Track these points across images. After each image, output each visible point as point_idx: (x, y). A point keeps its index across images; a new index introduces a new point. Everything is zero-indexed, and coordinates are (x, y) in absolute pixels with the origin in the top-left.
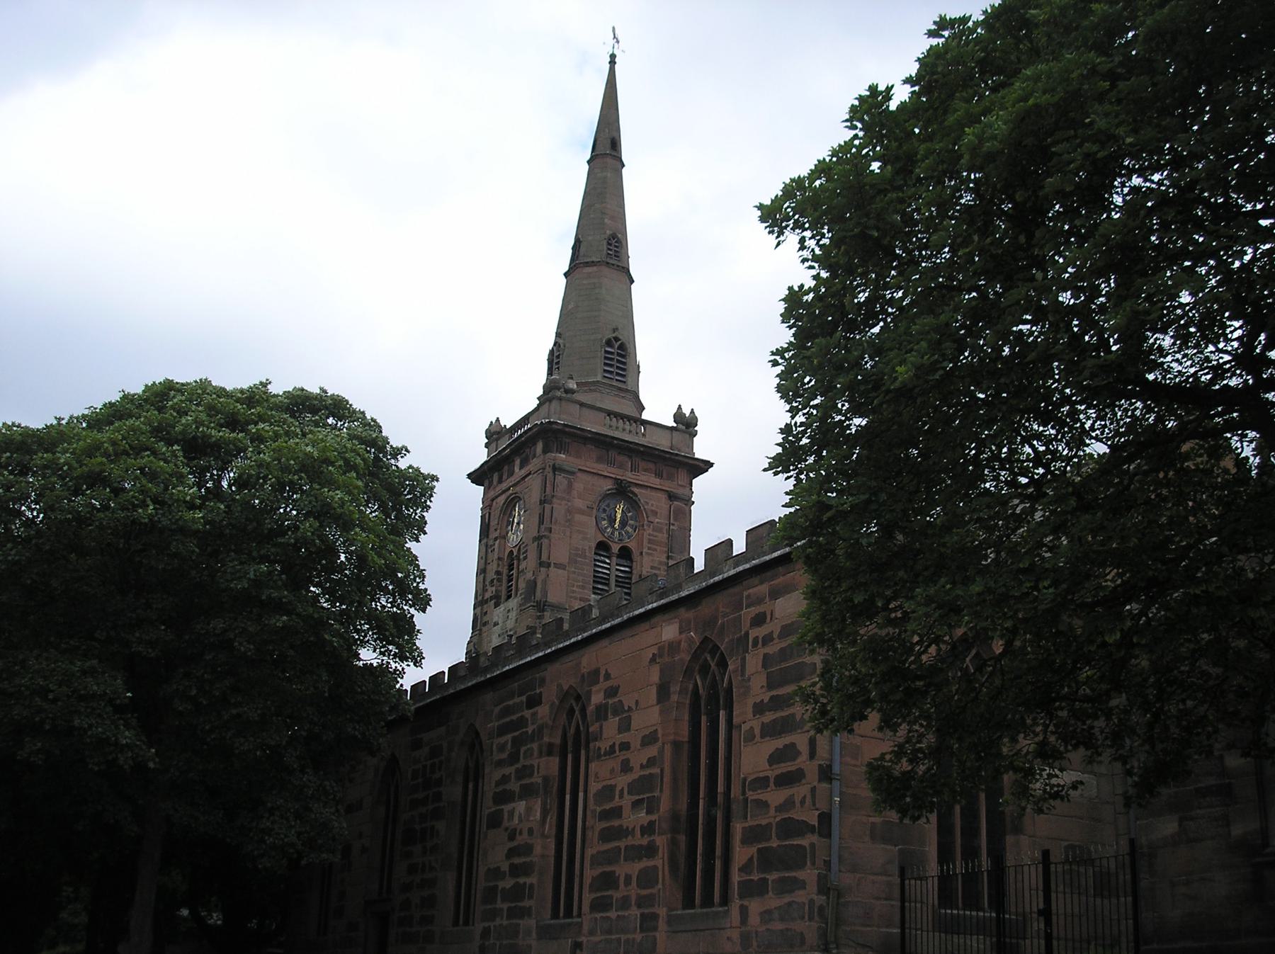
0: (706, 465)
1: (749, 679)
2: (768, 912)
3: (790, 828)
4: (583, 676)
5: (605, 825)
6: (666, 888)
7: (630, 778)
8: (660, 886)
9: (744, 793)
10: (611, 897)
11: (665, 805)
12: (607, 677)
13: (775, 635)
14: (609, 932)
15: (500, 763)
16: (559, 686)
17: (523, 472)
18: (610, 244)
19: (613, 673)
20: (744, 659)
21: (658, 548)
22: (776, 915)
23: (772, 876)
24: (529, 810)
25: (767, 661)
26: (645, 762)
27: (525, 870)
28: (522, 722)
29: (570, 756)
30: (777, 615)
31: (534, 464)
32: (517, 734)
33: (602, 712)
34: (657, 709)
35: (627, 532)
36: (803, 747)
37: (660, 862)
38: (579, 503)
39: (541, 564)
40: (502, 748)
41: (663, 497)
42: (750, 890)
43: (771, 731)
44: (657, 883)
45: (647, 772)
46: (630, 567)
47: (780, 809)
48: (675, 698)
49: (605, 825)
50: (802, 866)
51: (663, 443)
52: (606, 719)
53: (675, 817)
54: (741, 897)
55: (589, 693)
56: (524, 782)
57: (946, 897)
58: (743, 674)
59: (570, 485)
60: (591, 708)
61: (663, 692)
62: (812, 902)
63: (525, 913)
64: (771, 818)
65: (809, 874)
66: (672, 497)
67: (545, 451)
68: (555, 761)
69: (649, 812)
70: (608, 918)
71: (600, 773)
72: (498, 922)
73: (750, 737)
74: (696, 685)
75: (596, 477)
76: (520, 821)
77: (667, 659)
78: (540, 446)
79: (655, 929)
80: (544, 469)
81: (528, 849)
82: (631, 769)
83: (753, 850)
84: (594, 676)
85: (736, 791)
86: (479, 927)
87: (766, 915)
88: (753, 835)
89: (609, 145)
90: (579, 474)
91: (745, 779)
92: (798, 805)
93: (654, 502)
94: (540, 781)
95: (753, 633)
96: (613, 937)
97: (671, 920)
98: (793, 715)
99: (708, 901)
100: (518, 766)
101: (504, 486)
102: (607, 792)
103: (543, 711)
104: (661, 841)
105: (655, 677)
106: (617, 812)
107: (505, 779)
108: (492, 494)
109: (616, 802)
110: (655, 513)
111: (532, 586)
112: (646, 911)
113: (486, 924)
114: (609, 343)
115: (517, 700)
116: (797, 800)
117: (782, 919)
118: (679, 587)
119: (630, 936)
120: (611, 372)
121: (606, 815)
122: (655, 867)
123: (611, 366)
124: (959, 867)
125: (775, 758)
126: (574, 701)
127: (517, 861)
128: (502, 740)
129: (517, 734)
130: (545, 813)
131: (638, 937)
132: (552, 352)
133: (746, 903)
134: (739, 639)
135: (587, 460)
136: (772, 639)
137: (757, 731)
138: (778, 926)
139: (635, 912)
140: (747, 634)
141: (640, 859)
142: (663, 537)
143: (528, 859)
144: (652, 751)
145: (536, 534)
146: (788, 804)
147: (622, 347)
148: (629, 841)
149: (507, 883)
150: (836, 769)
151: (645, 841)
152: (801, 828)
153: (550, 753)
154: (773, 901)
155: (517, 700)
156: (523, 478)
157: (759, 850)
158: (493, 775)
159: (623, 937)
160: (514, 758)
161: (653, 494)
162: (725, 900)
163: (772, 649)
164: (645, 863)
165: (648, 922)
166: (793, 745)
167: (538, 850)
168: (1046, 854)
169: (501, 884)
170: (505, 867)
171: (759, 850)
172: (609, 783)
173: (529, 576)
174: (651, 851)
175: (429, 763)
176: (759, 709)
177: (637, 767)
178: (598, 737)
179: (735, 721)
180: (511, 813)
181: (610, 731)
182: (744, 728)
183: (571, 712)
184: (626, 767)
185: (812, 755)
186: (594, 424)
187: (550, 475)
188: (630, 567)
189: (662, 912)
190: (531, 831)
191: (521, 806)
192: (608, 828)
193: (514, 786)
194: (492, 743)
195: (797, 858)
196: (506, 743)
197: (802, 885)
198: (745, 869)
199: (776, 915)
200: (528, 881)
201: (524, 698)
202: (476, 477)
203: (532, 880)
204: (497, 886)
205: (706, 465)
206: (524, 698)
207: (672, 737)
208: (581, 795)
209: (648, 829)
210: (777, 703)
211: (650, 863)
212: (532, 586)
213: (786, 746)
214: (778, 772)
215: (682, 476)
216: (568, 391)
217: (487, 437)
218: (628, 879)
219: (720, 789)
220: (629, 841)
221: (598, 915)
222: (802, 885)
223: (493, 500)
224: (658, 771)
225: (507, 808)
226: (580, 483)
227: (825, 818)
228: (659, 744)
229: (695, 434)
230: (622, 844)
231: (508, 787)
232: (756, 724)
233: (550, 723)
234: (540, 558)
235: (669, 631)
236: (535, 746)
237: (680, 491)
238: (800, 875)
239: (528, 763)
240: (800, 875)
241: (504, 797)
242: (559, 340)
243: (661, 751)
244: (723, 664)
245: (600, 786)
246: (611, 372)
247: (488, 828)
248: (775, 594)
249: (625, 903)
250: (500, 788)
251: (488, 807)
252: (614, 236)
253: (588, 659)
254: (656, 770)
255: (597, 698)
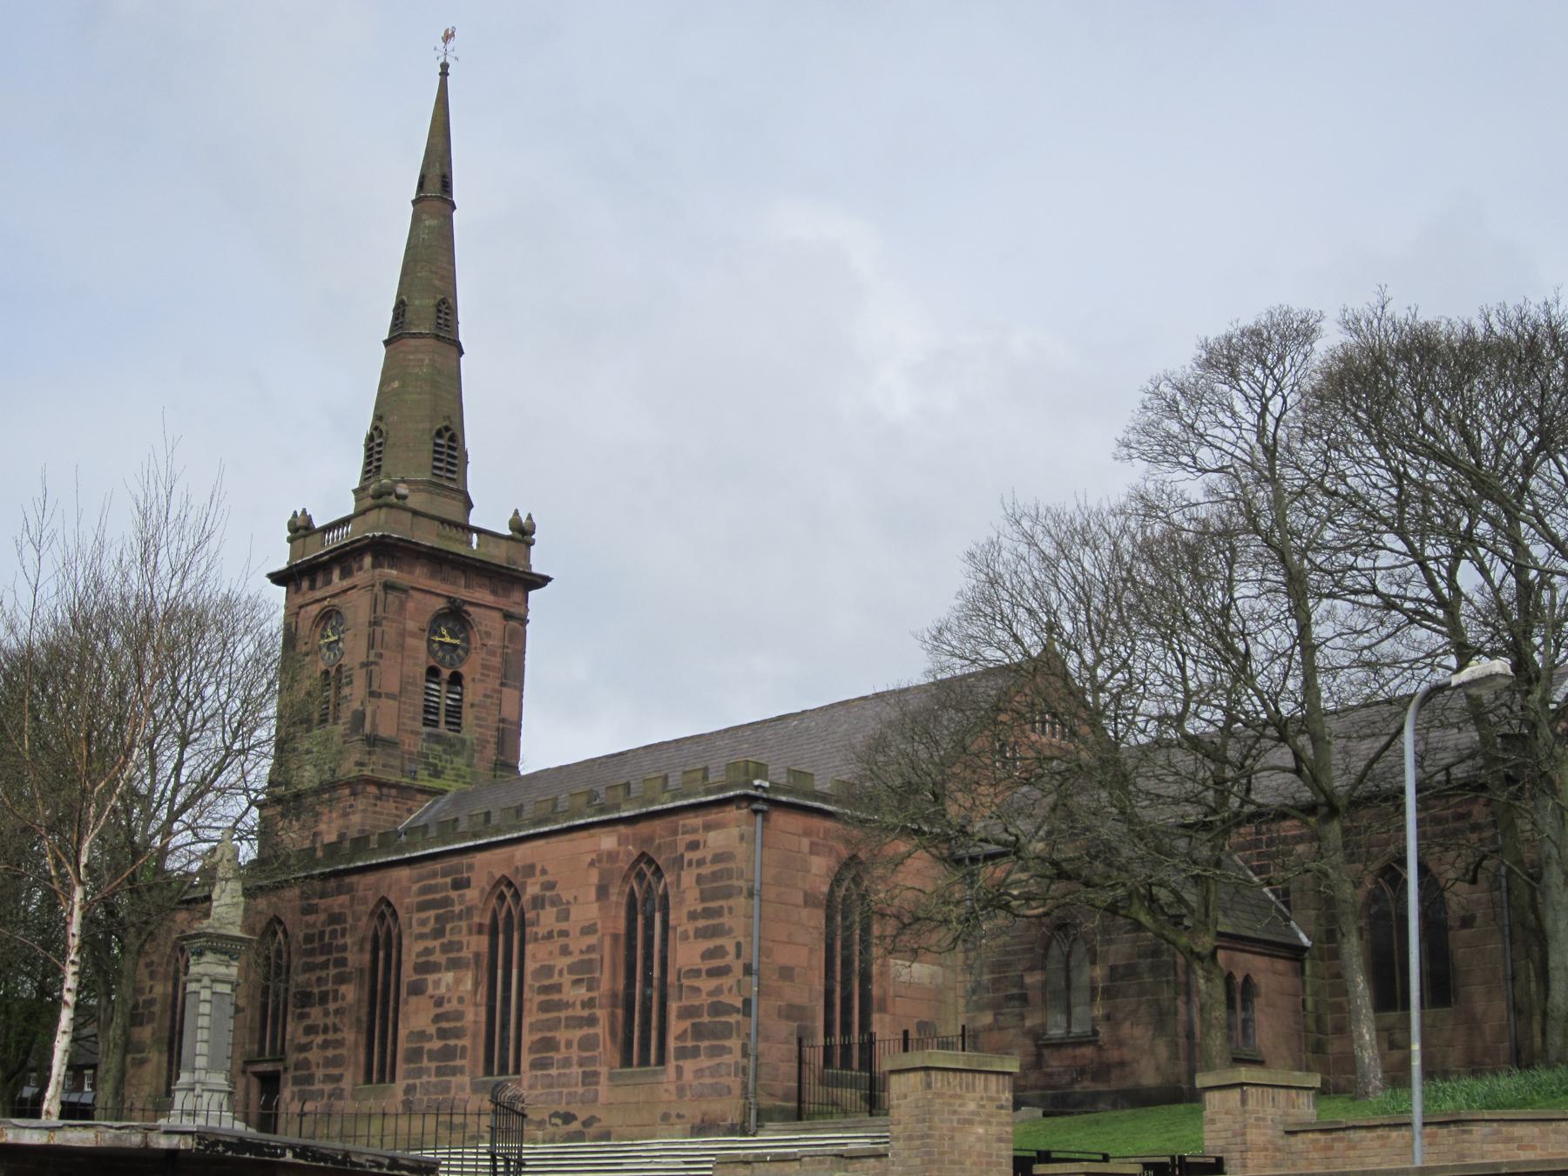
0: (543, 581)
1: (684, 892)
2: (701, 1070)
3: (718, 1009)
4: (517, 868)
5: (543, 997)
6: (607, 1052)
7: (568, 960)
8: (601, 1049)
9: (679, 979)
10: (552, 1058)
11: (605, 984)
12: (544, 872)
13: (708, 860)
14: (551, 1086)
15: (421, 936)
16: (490, 873)
17: (346, 583)
18: (439, 311)
19: (550, 869)
20: (679, 876)
21: (492, 674)
22: (707, 1073)
23: (704, 1044)
24: (458, 981)
25: (699, 879)
26: (584, 948)
27: (458, 1033)
28: (446, 902)
29: (501, 937)
30: (709, 843)
31: (360, 578)
32: (441, 911)
33: (538, 902)
34: (596, 906)
35: (458, 656)
36: (731, 949)
37: (601, 1030)
38: (411, 625)
39: (372, 694)
40: (423, 923)
41: (497, 615)
42: (682, 1053)
43: (702, 934)
44: (598, 1046)
45: (586, 957)
46: (461, 694)
47: (710, 994)
48: (613, 898)
49: (543, 997)
50: (729, 1036)
51: (498, 555)
52: (543, 907)
53: (614, 995)
54: (677, 1059)
55: (524, 885)
56: (452, 955)
57: (828, 1061)
58: (678, 886)
59: (402, 606)
60: (526, 898)
61: (602, 892)
62: (736, 1063)
63: (455, 1071)
64: (704, 1000)
65: (734, 1043)
66: (508, 616)
67: (374, 566)
68: (484, 940)
69: (590, 989)
70: (549, 1075)
71: (536, 955)
72: (425, 1079)
73: (685, 937)
74: (632, 888)
75: (428, 596)
76: (448, 990)
77: (605, 865)
78: (368, 561)
79: (597, 1083)
80: (373, 586)
81: (459, 1016)
82: (570, 953)
83: (687, 1024)
84: (530, 870)
85: (671, 978)
86: (400, 1084)
87: (699, 1073)
88: (686, 1013)
89: (438, 185)
90: (412, 592)
91: (680, 970)
92: (726, 992)
93: (487, 622)
94: (471, 956)
95: (688, 856)
96: (555, 1090)
97: (611, 1077)
98: (723, 924)
99: (644, 1061)
100: (445, 940)
101: (318, 594)
102: (547, 971)
103: (472, 895)
104: (602, 1014)
105: (594, 877)
106: (557, 988)
107: (428, 951)
108: (299, 600)
109: (555, 979)
110: (488, 634)
111: (359, 718)
112: (588, 1069)
113: (411, 1082)
114: (439, 434)
115: (440, 880)
116: (725, 988)
117: (712, 1076)
118: (617, 808)
119: (572, 1090)
120: (440, 469)
121: (545, 990)
122: (596, 1035)
123: (441, 460)
124: (837, 1039)
125: (708, 955)
126: (506, 887)
127: (445, 1025)
128: (424, 915)
129: (441, 911)
130: (476, 983)
131: (580, 1090)
132: (370, 438)
133: (681, 1063)
134: (675, 860)
135: (418, 576)
136: (705, 863)
137: (691, 933)
138: (708, 1080)
139: (576, 1071)
140: (682, 856)
141: (581, 1027)
142: (496, 661)
143: (458, 1024)
144: (592, 940)
145: (363, 659)
146: (718, 991)
147: (452, 438)
148: (570, 1012)
149: (437, 1044)
150: (755, 966)
151: (586, 1013)
152: (730, 1009)
153: (480, 932)
154: (704, 1062)
155: (440, 880)
156: (345, 591)
157: (693, 1024)
158: (412, 951)
159: (565, 1091)
160: (438, 933)
161: (487, 612)
162: (662, 1060)
163: (706, 870)
164: (586, 1031)
165: (590, 1078)
166: (722, 947)
167: (470, 1016)
168: (906, 1033)
169: (427, 1046)
170: (432, 1030)
171: (693, 1024)
172: (547, 963)
173: (356, 705)
174: (591, 1021)
175: (328, 929)
176: (693, 916)
177: (577, 952)
178: (536, 922)
179: (672, 923)
180: (437, 984)
181: (547, 919)
182: (679, 930)
183: (502, 897)
184: (565, 951)
185: (738, 955)
186: (427, 536)
187: (381, 595)
188: (461, 694)
189: (603, 1070)
190: (461, 1000)
191: (449, 977)
192: (547, 1001)
193: (438, 957)
194: (411, 919)
195: (726, 1031)
196: (428, 919)
197: (730, 1051)
198: (680, 1037)
199: (707, 1073)
200: (460, 1043)
201: (449, 880)
202: (277, 578)
203: (465, 1042)
204: (422, 1048)
205: (543, 581)
206: (449, 880)
207: (611, 931)
208: (515, 972)
209: (589, 1004)
210: (707, 913)
211: (591, 1031)
212: (359, 718)
213: (716, 947)
214: (710, 966)
215: (517, 596)
216: (399, 497)
217: (290, 530)
218: (569, 1044)
219: (656, 973)
220: (570, 1012)
221: (539, 1073)
222: (730, 1051)
223: (301, 607)
224: (598, 957)
225: (431, 978)
226: (415, 602)
227: (747, 1003)
228: (599, 934)
229: (531, 543)
230: (563, 1014)
231: (432, 958)
232: (690, 927)
233: (481, 906)
234: (370, 686)
235: (607, 841)
236: (464, 924)
237: (514, 610)
238: (727, 1043)
239: (456, 938)
240: (727, 1043)
241: (425, 967)
242: (378, 423)
243: (601, 940)
244: (658, 872)
245: (538, 965)
246: (440, 469)
247: (409, 994)
248: (708, 827)
249: (566, 1063)
250: (423, 959)
251: (408, 975)
252: (443, 301)
253: (522, 853)
254: (593, 956)
255: (532, 889)
